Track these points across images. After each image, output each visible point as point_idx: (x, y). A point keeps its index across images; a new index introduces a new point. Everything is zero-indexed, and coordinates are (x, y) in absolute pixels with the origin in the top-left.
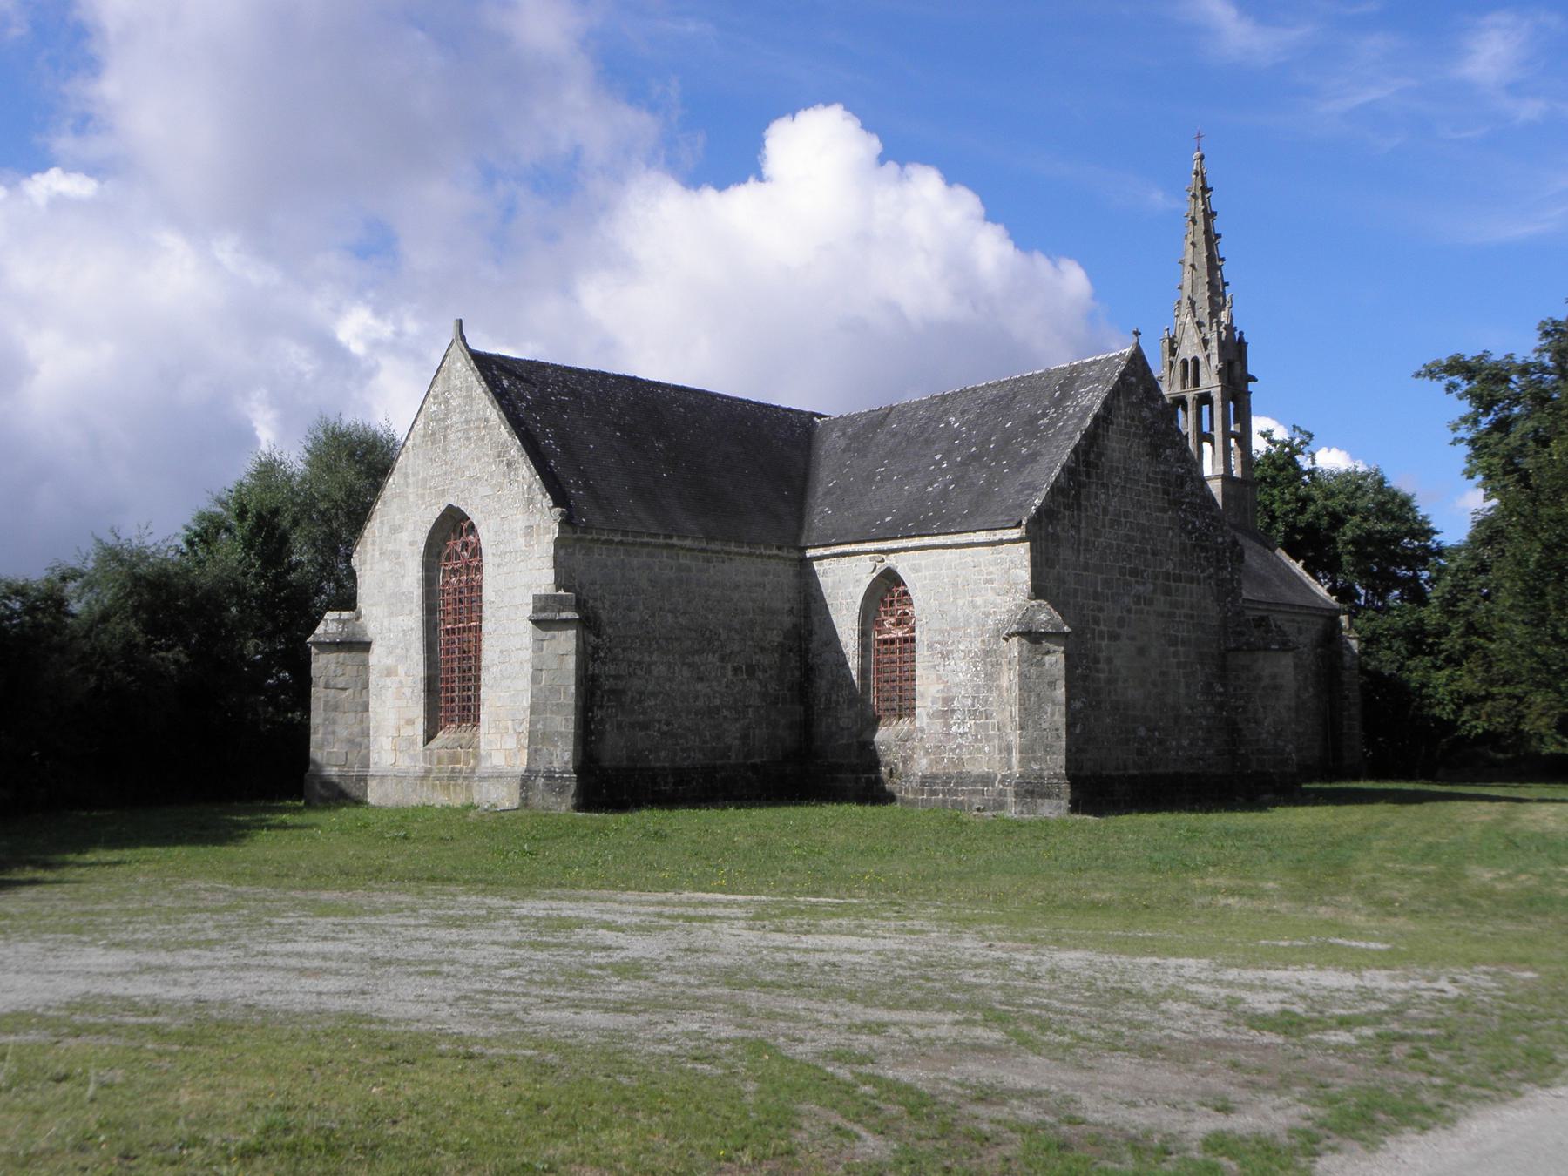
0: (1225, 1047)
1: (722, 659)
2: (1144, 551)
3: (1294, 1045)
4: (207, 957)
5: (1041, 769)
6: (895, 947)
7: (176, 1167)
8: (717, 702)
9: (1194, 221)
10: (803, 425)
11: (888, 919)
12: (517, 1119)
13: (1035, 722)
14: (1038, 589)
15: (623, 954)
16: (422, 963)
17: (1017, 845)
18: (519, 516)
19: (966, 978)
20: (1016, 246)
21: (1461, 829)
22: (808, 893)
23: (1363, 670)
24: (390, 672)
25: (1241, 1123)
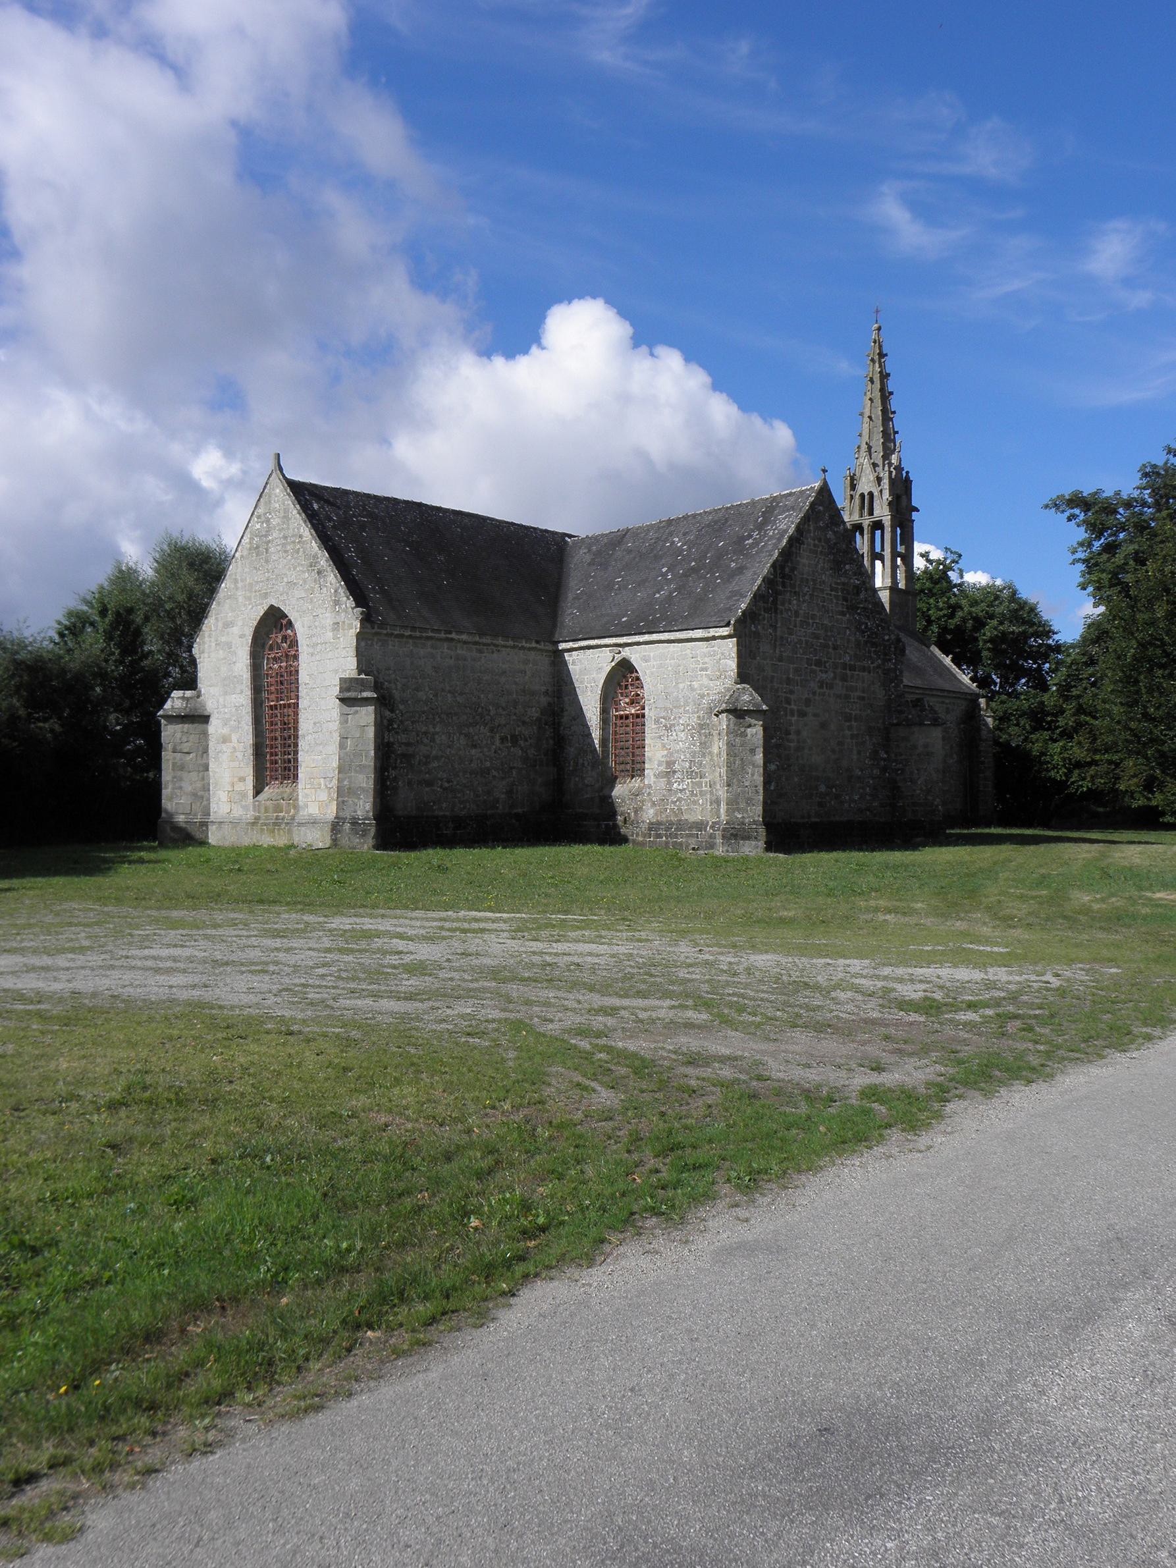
0: (880, 1025)
1: (492, 730)
2: (827, 646)
3: (933, 1022)
4: (81, 960)
5: (743, 817)
6: (626, 951)
7: (56, 1117)
8: (488, 764)
9: (872, 381)
10: (557, 544)
11: (621, 931)
12: (327, 1079)
13: (739, 781)
14: (743, 676)
15: (412, 957)
16: (253, 964)
17: (723, 876)
18: (327, 615)
19: (681, 975)
20: (739, 408)
21: (1068, 864)
22: (559, 912)
23: (996, 742)
24: (225, 740)
25: (888, 1079)
